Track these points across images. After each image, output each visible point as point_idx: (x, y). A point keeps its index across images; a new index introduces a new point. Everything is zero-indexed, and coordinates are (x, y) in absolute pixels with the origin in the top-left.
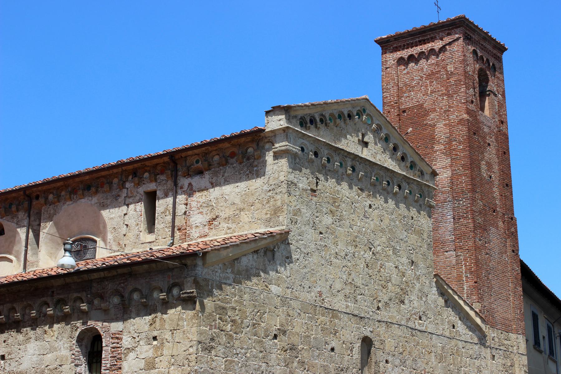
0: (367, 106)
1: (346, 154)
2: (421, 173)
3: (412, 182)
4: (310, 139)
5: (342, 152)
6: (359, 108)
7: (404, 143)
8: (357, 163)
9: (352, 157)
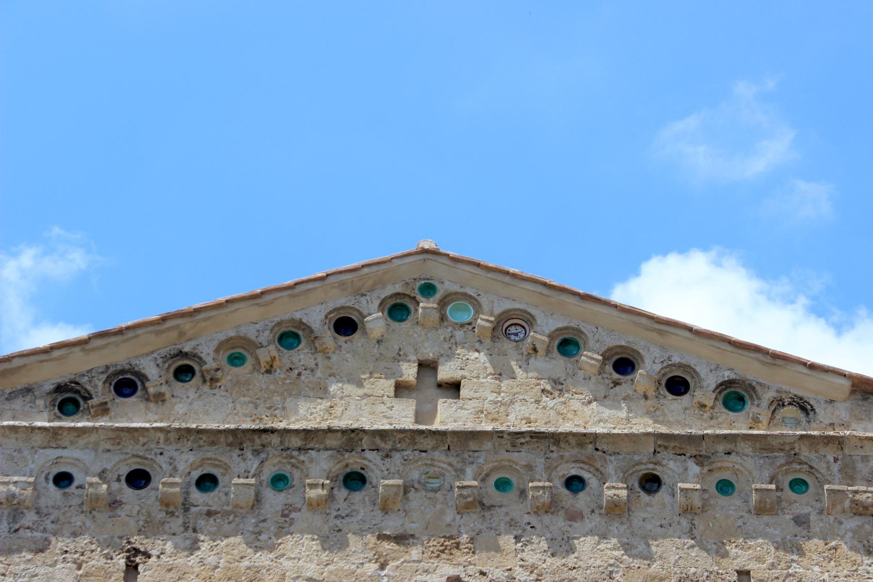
0: (437, 271)
1: (296, 442)
2: (803, 409)
3: (721, 448)
4: (93, 438)
5: (275, 439)
7: (661, 333)
8: (368, 454)
9: (332, 441)
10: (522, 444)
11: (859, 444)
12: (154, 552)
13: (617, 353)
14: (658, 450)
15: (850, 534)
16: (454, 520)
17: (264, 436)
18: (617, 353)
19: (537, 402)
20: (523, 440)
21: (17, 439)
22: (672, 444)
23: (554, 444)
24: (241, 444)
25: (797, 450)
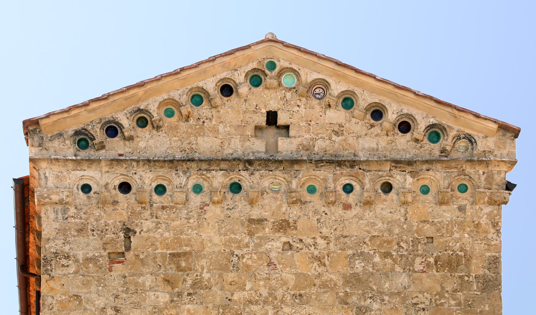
6: (254, 65)
10: (322, 166)
11: (497, 164)
12: (138, 230)
13: (374, 106)
14: (392, 168)
15: (486, 216)
16: (287, 210)
17: (188, 163)
18: (374, 106)
19: (330, 139)
20: (322, 164)
21: (59, 165)
22: (400, 165)
23: (338, 166)
24: (176, 167)
25: (464, 168)
